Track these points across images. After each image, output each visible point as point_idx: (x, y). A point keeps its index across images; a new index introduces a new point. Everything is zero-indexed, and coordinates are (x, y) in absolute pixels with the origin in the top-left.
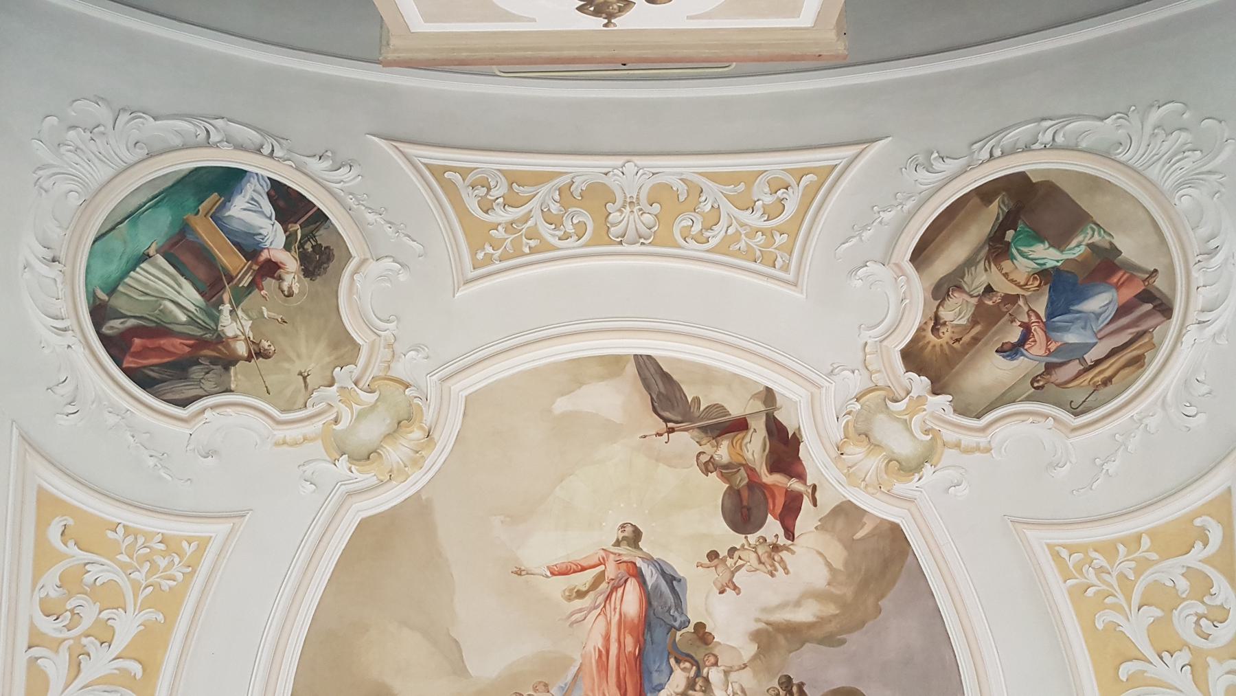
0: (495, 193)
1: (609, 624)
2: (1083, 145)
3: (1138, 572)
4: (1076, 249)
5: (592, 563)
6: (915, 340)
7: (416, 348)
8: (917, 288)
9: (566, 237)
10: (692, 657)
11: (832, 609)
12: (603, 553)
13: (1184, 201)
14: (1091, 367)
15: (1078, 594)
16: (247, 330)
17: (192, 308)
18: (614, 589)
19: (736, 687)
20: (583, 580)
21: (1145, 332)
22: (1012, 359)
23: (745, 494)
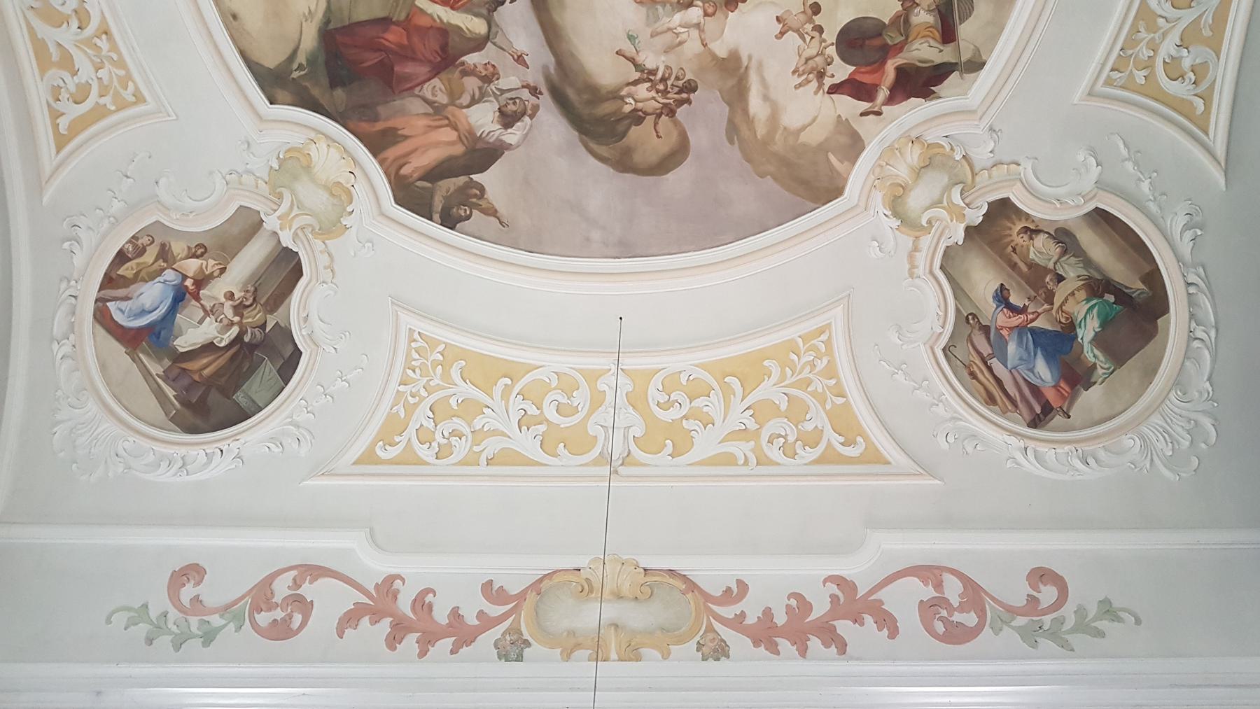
2: (1188, 363)
3: (814, 394)
4: (1091, 354)
6: (1018, 212)
8: (1069, 213)
11: (761, 131)
13: (1130, 442)
14: (985, 363)
19: (684, 36)
21: (1016, 406)
23: (877, 42)
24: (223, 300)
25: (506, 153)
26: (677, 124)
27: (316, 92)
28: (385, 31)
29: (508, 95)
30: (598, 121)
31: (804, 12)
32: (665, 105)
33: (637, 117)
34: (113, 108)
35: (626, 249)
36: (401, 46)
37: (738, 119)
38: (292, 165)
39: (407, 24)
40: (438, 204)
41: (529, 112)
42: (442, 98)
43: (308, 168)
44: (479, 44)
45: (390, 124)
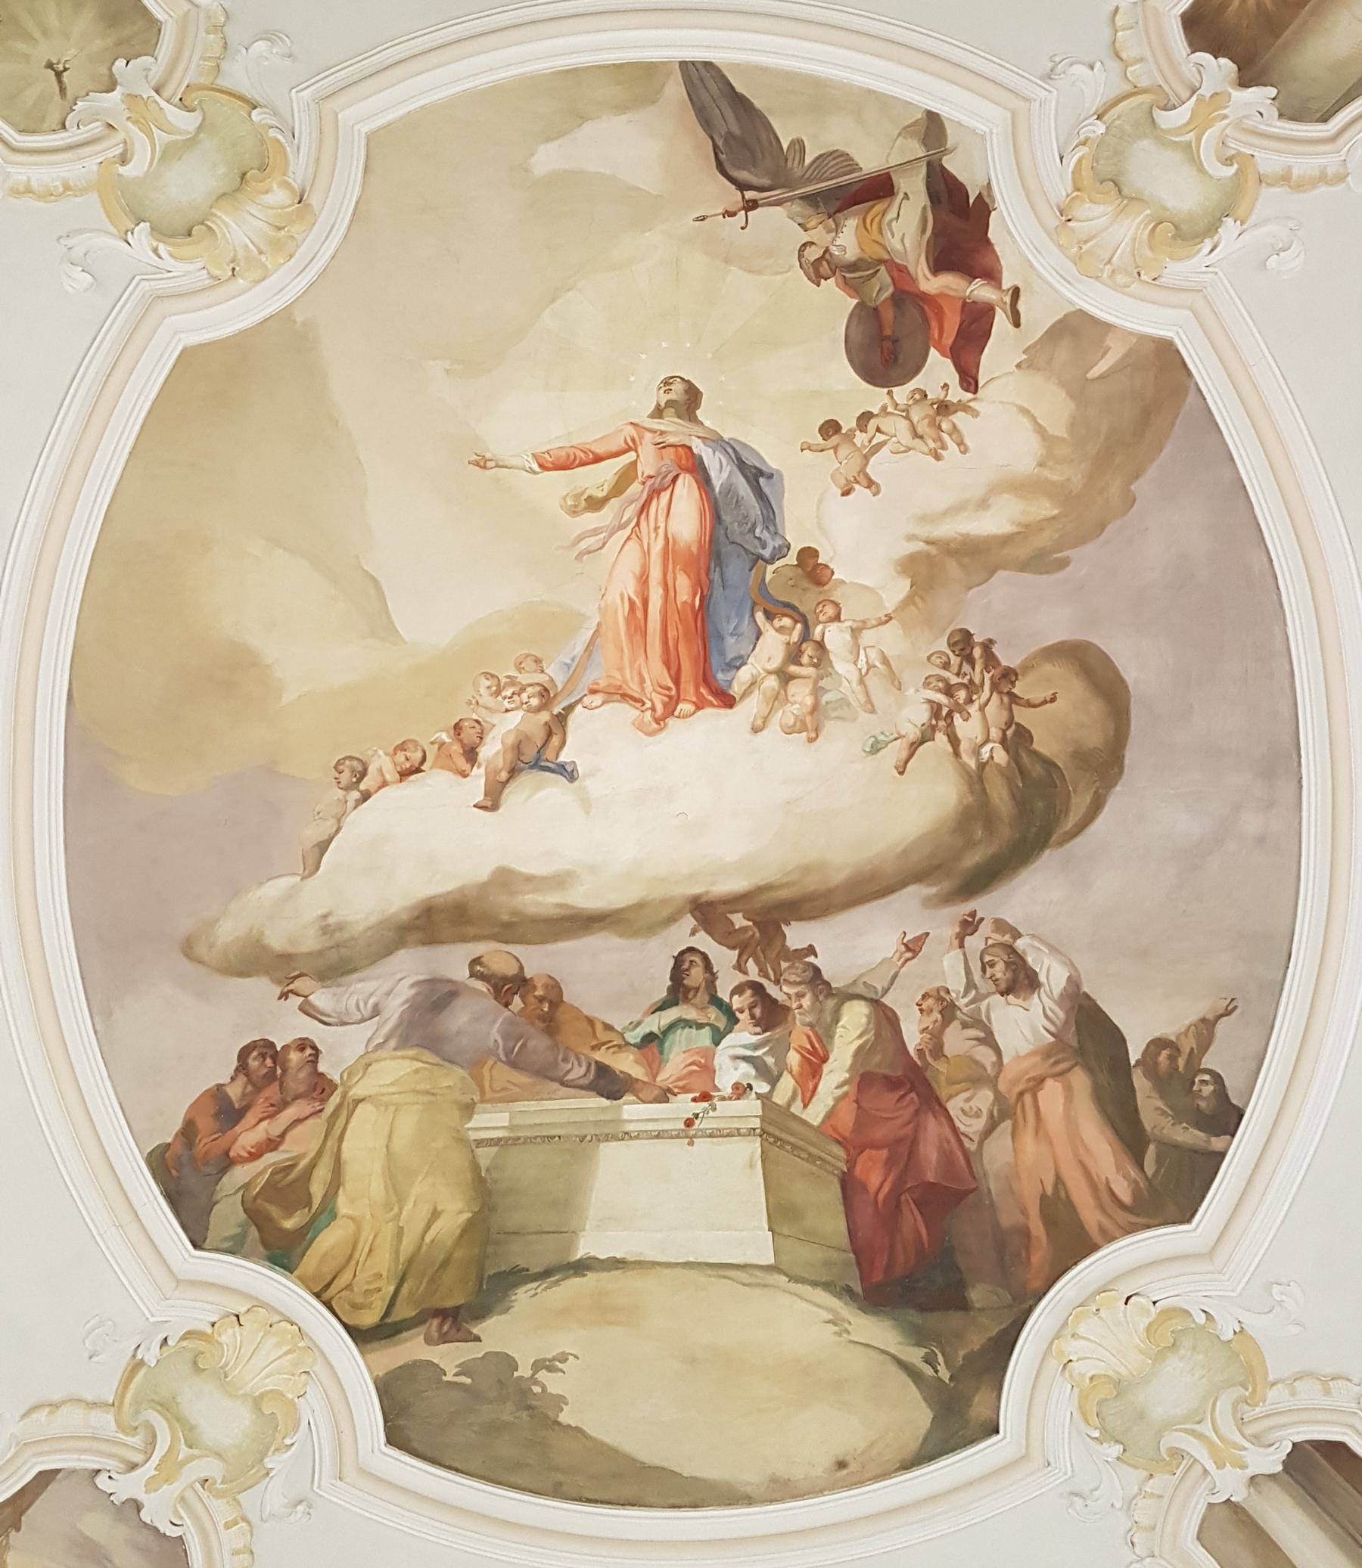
1: (646, 554)
5: (614, 448)
7: (270, 36)
11: (1045, 509)
18: (655, 493)
19: (873, 654)
23: (888, 315)
25: (1085, 989)
26: (1028, 666)
27: (976, 1341)
28: (864, 1187)
29: (977, 976)
30: (1025, 811)
31: (835, 448)
32: (994, 687)
33: (1017, 739)
35: (1281, 762)
36: (890, 1163)
37: (1022, 552)
38: (1111, 1411)
39: (855, 1145)
40: (1189, 1136)
41: (1007, 938)
43: (1120, 1387)
44: (885, 1020)
45: (1034, 1211)
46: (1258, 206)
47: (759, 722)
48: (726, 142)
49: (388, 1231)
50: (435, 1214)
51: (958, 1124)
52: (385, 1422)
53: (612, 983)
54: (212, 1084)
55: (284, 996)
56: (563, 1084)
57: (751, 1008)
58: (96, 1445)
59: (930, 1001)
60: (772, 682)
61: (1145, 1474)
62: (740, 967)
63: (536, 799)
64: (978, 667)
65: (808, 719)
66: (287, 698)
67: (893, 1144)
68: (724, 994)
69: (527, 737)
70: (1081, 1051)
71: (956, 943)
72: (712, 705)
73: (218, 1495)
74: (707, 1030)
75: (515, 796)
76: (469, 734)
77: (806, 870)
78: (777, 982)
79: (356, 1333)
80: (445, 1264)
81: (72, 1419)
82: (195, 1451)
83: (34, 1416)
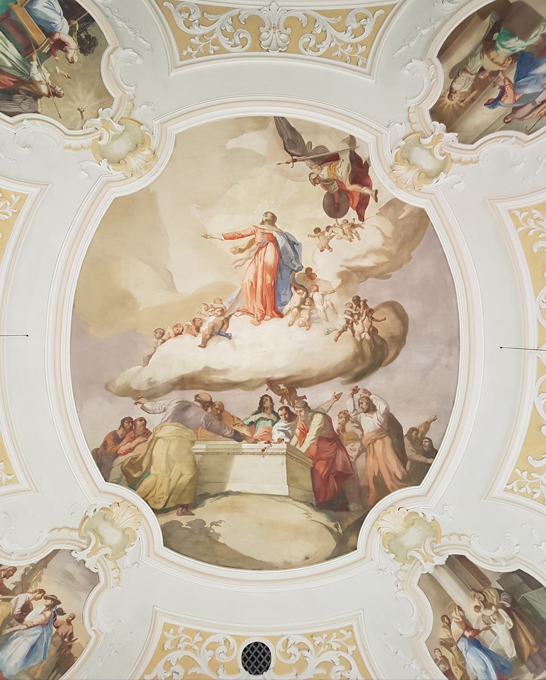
0: (193, 17)
1: (257, 268)
5: (248, 233)
6: (438, 103)
7: (147, 103)
9: (235, 45)
10: (304, 287)
11: (384, 259)
12: (254, 228)
14: (539, 106)
15: (524, 235)
16: (47, 79)
17: (15, 60)
18: (261, 248)
19: (328, 303)
20: (243, 243)
22: (494, 108)
23: (337, 196)
24: (479, 614)
25: (391, 412)
26: (377, 309)
27: (351, 521)
28: (318, 472)
29: (357, 407)
30: (375, 355)
31: (319, 237)
32: (367, 315)
33: (373, 332)
34: (355, 647)
35: (454, 342)
36: (327, 465)
37: (376, 272)
38: (392, 544)
39: (316, 459)
40: (421, 458)
41: (367, 395)
42: (357, 445)
43: (395, 536)
44: (327, 420)
46: (451, 169)
47: (291, 323)
48: (287, 141)
49: (167, 479)
50: (181, 475)
51: (349, 453)
52: (164, 539)
53: (240, 405)
54: (113, 430)
55: (136, 403)
56: (223, 436)
57: (285, 415)
58: (73, 542)
59: (342, 414)
60: (296, 310)
61: (402, 564)
62: (282, 401)
63: (218, 345)
64: (362, 308)
65: (307, 323)
66: (140, 309)
67: (328, 459)
68: (276, 410)
69: (216, 325)
70: (388, 431)
71: (351, 396)
72: (276, 317)
73: (109, 559)
74: (270, 422)
75: (212, 343)
76: (198, 323)
77: (304, 371)
78: (293, 407)
79: (155, 510)
80: (184, 491)
81: (65, 533)
82: (103, 545)
83: (53, 532)
